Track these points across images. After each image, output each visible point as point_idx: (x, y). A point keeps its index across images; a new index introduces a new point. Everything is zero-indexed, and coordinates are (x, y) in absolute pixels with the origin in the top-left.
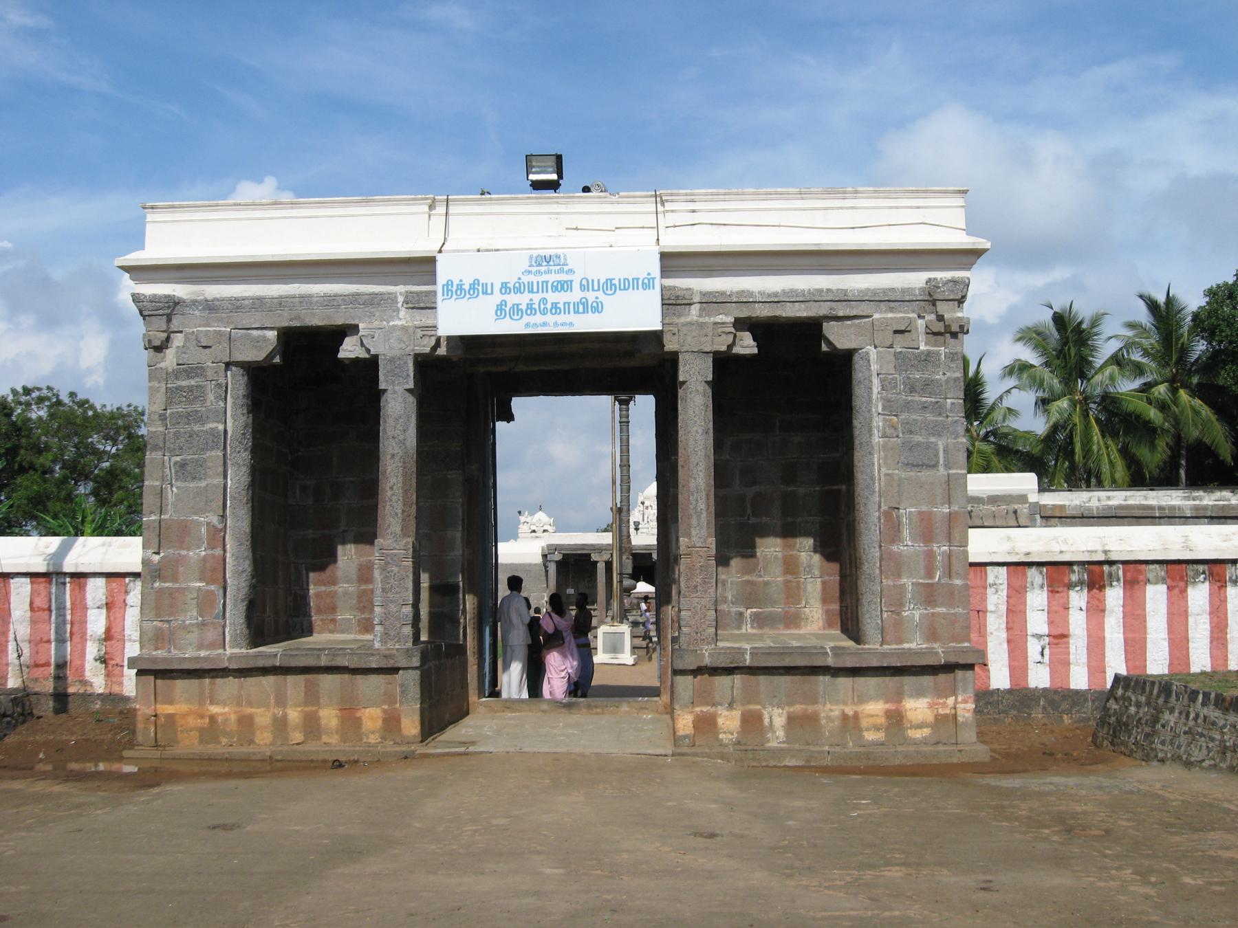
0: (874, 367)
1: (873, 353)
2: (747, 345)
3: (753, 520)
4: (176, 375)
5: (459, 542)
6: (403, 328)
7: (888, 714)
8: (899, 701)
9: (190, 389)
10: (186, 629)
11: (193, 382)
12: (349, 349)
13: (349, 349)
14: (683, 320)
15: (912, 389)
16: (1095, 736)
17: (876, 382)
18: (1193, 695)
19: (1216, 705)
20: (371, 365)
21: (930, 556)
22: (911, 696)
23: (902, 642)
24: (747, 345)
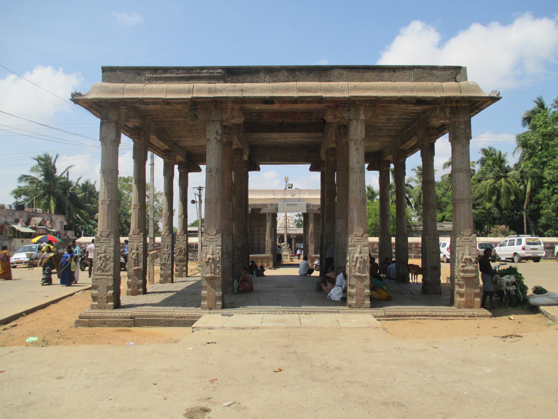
12: (261, 212)
13: (261, 212)
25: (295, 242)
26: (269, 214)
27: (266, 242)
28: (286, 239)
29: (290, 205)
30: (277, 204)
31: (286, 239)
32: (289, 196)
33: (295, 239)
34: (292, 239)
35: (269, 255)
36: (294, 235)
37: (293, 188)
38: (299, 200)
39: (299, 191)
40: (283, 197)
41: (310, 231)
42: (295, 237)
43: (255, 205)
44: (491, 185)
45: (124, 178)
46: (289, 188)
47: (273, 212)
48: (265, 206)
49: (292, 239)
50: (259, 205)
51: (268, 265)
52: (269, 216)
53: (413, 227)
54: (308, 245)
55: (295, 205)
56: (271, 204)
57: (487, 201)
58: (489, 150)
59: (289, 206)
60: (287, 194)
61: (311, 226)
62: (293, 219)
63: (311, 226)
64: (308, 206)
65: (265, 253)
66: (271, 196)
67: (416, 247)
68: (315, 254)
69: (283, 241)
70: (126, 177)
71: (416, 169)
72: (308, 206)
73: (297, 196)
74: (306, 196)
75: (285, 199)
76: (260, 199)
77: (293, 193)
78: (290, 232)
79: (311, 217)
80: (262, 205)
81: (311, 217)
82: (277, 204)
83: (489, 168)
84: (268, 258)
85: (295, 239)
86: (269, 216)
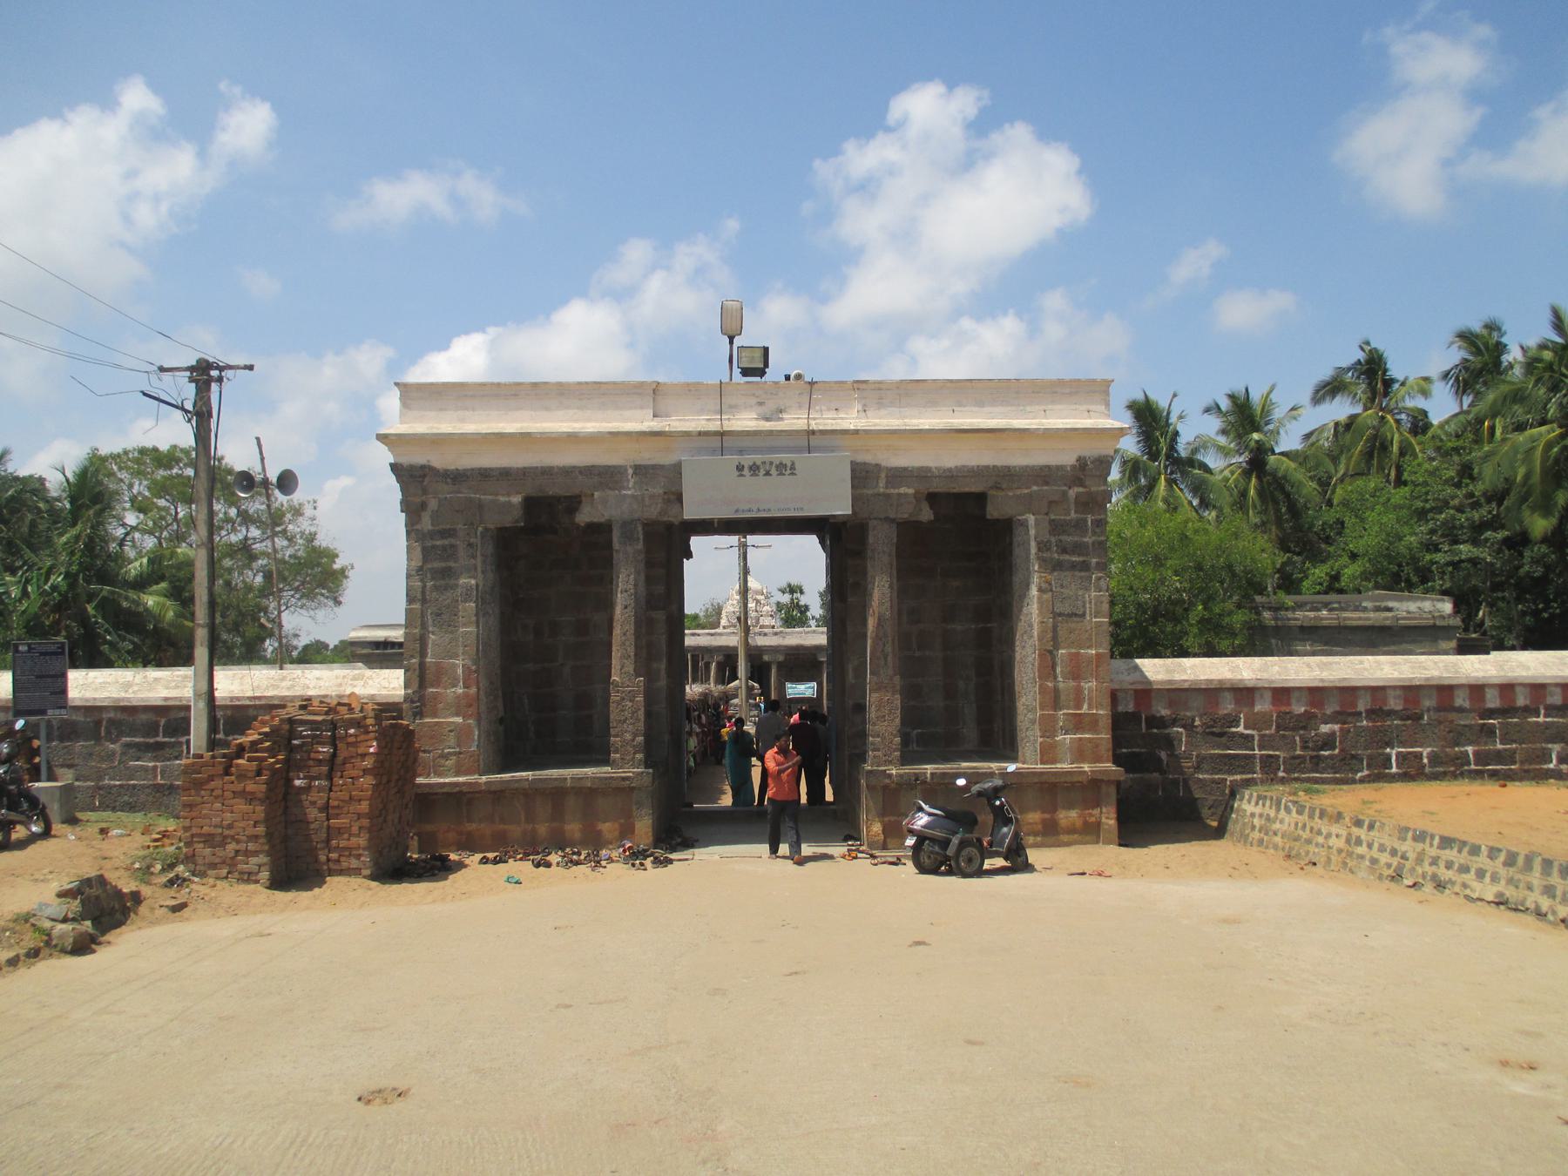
0: (1032, 532)
1: (1031, 519)
2: (926, 514)
3: (917, 654)
4: (432, 535)
5: (663, 673)
6: (633, 496)
7: (1044, 821)
8: (1054, 810)
9: (444, 548)
10: (446, 757)
11: (446, 542)
12: (584, 516)
13: (584, 516)
14: (870, 492)
15: (1064, 551)
16: (1340, 534)
17: (1033, 544)
18: (1547, 864)
19: (1321, 818)
20: (601, 530)
21: (1079, 691)
22: (1063, 808)
23: (1054, 762)
24: (926, 514)
25: (778, 675)
26: (627, 525)
27: (614, 697)
28: (742, 668)
29: (754, 469)
30: (677, 469)
31: (742, 668)
32: (745, 421)
33: (780, 665)
34: (768, 666)
35: (629, 772)
36: (774, 650)
37: (774, 374)
38: (810, 440)
39: (809, 389)
40: (714, 426)
41: (871, 623)
42: (781, 658)
43: (547, 472)
44: (1549, 445)
45: (155, 450)
46: (746, 372)
47: (653, 512)
48: (608, 476)
49: (768, 666)
50: (567, 472)
51: (627, 831)
52: (628, 537)
53: (1267, 615)
54: (861, 708)
55: (781, 467)
56: (639, 470)
57: (1533, 509)
58: (1485, 332)
59: (748, 478)
60: (734, 408)
61: (880, 593)
62: (773, 600)
63: (880, 593)
64: (862, 475)
65: (606, 761)
66: (639, 421)
67: (1438, 709)
68: (905, 760)
69: (734, 677)
70: (164, 447)
71: (1225, 404)
72: (862, 475)
73: (794, 421)
74: (851, 419)
75: (722, 434)
76: (573, 438)
77: (771, 405)
78: (761, 641)
79: (881, 541)
80: (588, 471)
81: (881, 541)
82: (677, 469)
83: (1547, 375)
84: (621, 790)
85: (780, 665)
86: (628, 537)
